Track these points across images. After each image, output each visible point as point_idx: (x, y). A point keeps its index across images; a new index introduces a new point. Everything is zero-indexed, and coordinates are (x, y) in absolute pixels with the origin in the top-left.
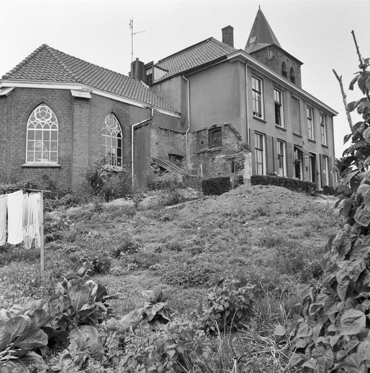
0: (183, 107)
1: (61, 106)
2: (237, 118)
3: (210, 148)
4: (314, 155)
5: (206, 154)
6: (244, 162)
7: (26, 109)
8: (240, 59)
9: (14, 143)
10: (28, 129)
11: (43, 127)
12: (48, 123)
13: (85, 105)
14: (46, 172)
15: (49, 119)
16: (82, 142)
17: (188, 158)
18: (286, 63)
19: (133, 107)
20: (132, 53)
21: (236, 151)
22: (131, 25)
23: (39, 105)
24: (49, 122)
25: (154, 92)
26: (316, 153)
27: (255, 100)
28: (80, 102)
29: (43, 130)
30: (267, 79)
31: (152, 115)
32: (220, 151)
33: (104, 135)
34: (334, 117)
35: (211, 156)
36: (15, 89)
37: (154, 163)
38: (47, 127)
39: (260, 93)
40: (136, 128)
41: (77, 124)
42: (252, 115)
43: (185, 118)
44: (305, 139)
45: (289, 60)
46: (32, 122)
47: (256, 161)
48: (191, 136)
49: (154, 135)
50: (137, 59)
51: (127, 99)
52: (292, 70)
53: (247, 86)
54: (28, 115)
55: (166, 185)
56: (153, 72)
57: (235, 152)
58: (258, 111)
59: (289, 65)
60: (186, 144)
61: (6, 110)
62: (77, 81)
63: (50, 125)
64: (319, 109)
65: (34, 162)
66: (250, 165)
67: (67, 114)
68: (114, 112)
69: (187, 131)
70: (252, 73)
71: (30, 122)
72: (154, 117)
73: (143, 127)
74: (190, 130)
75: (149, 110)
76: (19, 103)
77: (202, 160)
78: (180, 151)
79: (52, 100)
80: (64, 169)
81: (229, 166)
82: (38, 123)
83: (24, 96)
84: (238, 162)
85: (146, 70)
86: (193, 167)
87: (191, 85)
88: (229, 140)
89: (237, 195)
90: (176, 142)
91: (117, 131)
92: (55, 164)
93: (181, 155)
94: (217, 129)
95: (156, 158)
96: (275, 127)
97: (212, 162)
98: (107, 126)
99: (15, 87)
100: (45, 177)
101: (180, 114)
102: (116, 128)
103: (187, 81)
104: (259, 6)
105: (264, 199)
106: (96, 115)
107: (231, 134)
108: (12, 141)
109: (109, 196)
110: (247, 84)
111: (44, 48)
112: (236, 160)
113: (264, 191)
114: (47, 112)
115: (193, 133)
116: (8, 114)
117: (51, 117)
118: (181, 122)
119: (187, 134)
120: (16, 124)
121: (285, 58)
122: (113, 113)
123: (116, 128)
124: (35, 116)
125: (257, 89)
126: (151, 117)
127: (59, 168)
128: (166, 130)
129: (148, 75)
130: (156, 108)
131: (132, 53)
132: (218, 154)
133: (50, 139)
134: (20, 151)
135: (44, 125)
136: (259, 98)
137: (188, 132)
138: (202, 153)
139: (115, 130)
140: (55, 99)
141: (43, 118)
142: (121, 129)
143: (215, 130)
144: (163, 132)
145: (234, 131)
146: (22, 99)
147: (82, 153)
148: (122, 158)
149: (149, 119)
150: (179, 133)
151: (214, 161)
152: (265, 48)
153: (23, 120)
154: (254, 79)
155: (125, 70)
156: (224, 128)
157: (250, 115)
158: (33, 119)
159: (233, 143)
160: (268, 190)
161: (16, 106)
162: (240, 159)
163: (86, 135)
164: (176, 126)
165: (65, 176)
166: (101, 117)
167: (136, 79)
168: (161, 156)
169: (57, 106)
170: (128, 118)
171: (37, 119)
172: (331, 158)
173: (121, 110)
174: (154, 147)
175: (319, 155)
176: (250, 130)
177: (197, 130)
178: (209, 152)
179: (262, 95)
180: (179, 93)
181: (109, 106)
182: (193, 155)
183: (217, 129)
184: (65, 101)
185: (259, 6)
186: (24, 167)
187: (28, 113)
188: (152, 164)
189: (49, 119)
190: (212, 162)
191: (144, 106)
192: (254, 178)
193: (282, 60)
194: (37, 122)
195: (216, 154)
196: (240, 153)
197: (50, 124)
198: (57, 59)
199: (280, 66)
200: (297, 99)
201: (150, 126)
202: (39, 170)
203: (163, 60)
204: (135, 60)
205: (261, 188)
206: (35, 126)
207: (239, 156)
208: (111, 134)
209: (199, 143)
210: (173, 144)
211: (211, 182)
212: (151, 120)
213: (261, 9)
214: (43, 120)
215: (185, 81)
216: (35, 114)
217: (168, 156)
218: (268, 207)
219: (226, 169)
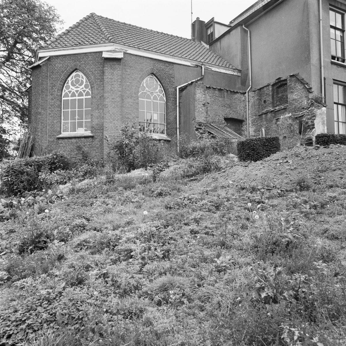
0: (244, 61)
1: (94, 71)
2: (307, 64)
3: (274, 107)
6: (315, 119)
7: (60, 77)
9: (50, 114)
10: (63, 99)
11: (77, 95)
12: (81, 90)
13: (117, 66)
14: (81, 143)
15: (83, 86)
16: (114, 107)
17: (249, 121)
19: (178, 66)
20: (192, 13)
21: (305, 108)
23: (73, 72)
24: (83, 89)
25: (214, 51)
27: (336, 40)
28: (111, 63)
29: (77, 98)
31: (203, 74)
32: (285, 109)
35: (274, 117)
36: (50, 58)
37: (200, 127)
38: (81, 94)
39: (342, 31)
40: (182, 90)
41: (108, 88)
42: (330, 60)
43: (247, 75)
46: (67, 91)
47: (336, 119)
48: (252, 96)
49: (200, 95)
50: (198, 18)
51: (170, 57)
53: (321, 21)
54: (62, 84)
55: (193, 153)
56: (214, 29)
57: (303, 108)
58: (339, 55)
60: (246, 106)
61: (40, 81)
63: (84, 93)
65: (69, 133)
66: (323, 124)
67: (99, 79)
68: (155, 73)
69: (248, 90)
70: (330, 5)
72: (206, 76)
73: (188, 88)
74: (251, 88)
75: (199, 68)
76: (53, 72)
77: (265, 123)
78: (240, 114)
79: (85, 65)
80: (96, 139)
81: (297, 127)
82: (73, 91)
83: (58, 65)
84: (307, 120)
85: (207, 29)
86: (255, 131)
87: (252, 34)
89: (278, 160)
90: (234, 104)
91: (159, 94)
92: (89, 133)
93: (240, 118)
94: (282, 83)
95: (202, 121)
97: (276, 123)
99: (50, 56)
100: (79, 148)
101: (240, 71)
102: (157, 90)
103: (248, 31)
105: (316, 165)
106: (132, 78)
107: (299, 87)
108: (49, 112)
109: (132, 167)
110: (321, 18)
111: (92, 16)
112: (304, 119)
113: (320, 153)
114: (80, 79)
115: (254, 91)
116: (42, 84)
117: (84, 84)
118: (242, 81)
119: (247, 93)
120: (52, 95)
122: (153, 74)
123: (157, 90)
124: (70, 84)
125: (339, 26)
126: (202, 76)
128: (220, 90)
129: (209, 34)
130: (208, 65)
131: (192, 13)
132: (283, 113)
133: (84, 108)
134: (55, 122)
135: (78, 93)
137: (249, 90)
138: (264, 114)
139: (157, 93)
140: (88, 64)
142: (164, 92)
144: (217, 92)
145: (302, 82)
146: (57, 68)
147: (114, 120)
149: (199, 78)
150: (237, 92)
151: (278, 123)
154: (334, 13)
155: (187, 34)
156: (290, 81)
157: (326, 60)
158: (68, 88)
159: (301, 98)
160: (327, 150)
161: (51, 75)
162: (309, 116)
163: (118, 99)
164: (235, 85)
165: (98, 146)
167: (196, 40)
168: (214, 121)
169: (89, 71)
170: (172, 79)
171: (71, 87)
174: (201, 109)
176: (325, 79)
177: (259, 88)
178: (272, 111)
180: (239, 46)
181: (148, 67)
182: (254, 117)
183: (282, 83)
184: (97, 65)
186: (59, 138)
187: (62, 82)
188: (197, 129)
189: (83, 86)
190: (276, 123)
191: (192, 64)
192: (320, 137)
194: (71, 90)
195: (281, 114)
196: (310, 109)
197: (84, 91)
201: (195, 85)
202: (74, 140)
205: (317, 148)
207: (308, 113)
208: (152, 98)
209: (261, 102)
210: (230, 106)
211: (248, 144)
212: (201, 79)
214: (77, 87)
215: (246, 32)
216: (70, 82)
218: (320, 177)
219: (292, 131)
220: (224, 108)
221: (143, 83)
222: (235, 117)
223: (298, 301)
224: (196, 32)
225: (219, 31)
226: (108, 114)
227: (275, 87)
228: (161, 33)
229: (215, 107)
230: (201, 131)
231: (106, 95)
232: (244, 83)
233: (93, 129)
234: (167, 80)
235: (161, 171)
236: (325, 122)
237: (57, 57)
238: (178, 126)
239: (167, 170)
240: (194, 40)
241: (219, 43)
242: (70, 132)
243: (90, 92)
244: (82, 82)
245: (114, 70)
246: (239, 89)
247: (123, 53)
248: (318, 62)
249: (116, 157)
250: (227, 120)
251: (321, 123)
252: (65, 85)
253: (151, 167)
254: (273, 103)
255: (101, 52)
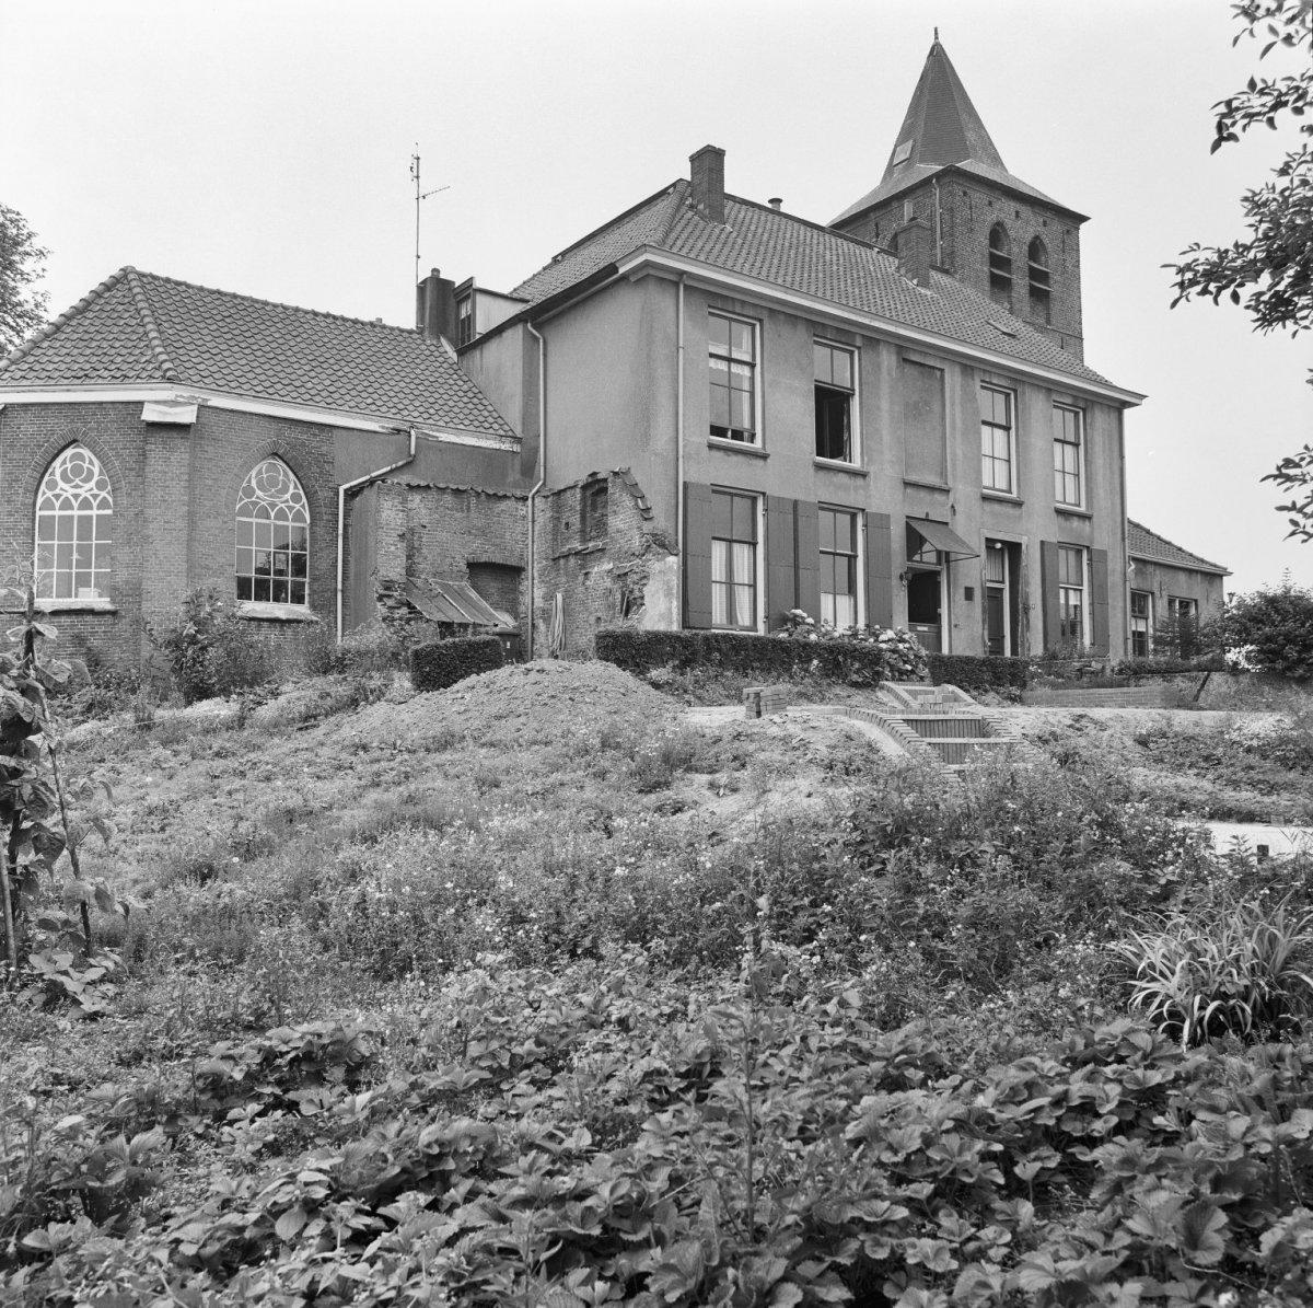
0: (529, 416)
3: (584, 540)
4: (1014, 549)
5: (572, 561)
8: (652, 272)
10: (38, 513)
11: (76, 505)
13: (179, 442)
14: (80, 625)
15: (92, 484)
16: (170, 543)
17: (535, 569)
18: (1009, 222)
19: (343, 432)
22: (415, 170)
26: (1024, 540)
29: (76, 513)
30: (782, 317)
31: (413, 452)
32: (602, 550)
33: (285, 523)
34: (1127, 412)
38: (86, 504)
39: (752, 366)
40: (352, 494)
43: (537, 450)
44: (963, 493)
45: (1025, 211)
46: (49, 494)
48: (542, 507)
50: (435, 271)
52: (1035, 249)
54: (38, 476)
59: (1021, 229)
62: (163, 377)
64: (1049, 390)
65: (54, 600)
66: (668, 594)
68: (280, 452)
71: (44, 493)
73: (366, 492)
74: (544, 484)
75: (402, 436)
77: (564, 580)
82: (65, 494)
83: (27, 427)
85: (459, 303)
88: (621, 519)
91: (291, 504)
92: (103, 603)
93: (513, 562)
95: (395, 579)
96: (812, 470)
98: (259, 493)
100: (79, 640)
101: (518, 440)
102: (288, 496)
104: (936, 30)
107: (628, 501)
109: (201, 692)
114: (86, 465)
117: (96, 478)
121: (1005, 210)
123: (288, 496)
124: (58, 477)
127: (114, 613)
128: (457, 492)
136: (752, 379)
141: (77, 481)
143: (596, 489)
144: (448, 498)
145: (635, 491)
147: (169, 573)
148: (307, 580)
149: (400, 463)
150: (505, 497)
151: (588, 583)
152: (926, 182)
153: (26, 490)
155: (403, 313)
158: (52, 485)
163: (181, 524)
166: (236, 470)
167: (426, 333)
171: (61, 484)
172: (1104, 553)
173: (303, 443)
174: (393, 548)
175: (1038, 546)
179: (758, 369)
181: (264, 438)
185: (936, 30)
188: (380, 598)
189: (92, 484)
193: (991, 217)
197: (95, 496)
198: (142, 312)
199: (983, 239)
200: (933, 368)
203: (563, 254)
204: (429, 275)
206: (57, 504)
209: (558, 528)
210: (483, 532)
212: (408, 464)
213: (941, 40)
214: (77, 486)
215: (536, 339)
216: (58, 473)
217: (464, 568)
220: (467, 538)
221: (249, 482)
222: (498, 559)
223: (631, 1030)
224: (428, 305)
225: (487, 316)
226: (153, 560)
227: (589, 493)
228: (323, 315)
229: (443, 536)
230: (390, 602)
231: (149, 512)
232: (528, 469)
233: (113, 591)
234: (314, 468)
235: (260, 704)
236: (675, 591)
237: (26, 406)
238: (340, 586)
239: (271, 702)
240: (421, 331)
241: (478, 353)
242: (57, 596)
243: (111, 500)
244: (90, 474)
245: (172, 450)
246: (516, 485)
247: (196, 407)
248: (671, 446)
249: (167, 667)
250: (476, 568)
251: (661, 593)
252: (46, 478)
253: (240, 694)
254: (583, 531)
255: (141, 403)
